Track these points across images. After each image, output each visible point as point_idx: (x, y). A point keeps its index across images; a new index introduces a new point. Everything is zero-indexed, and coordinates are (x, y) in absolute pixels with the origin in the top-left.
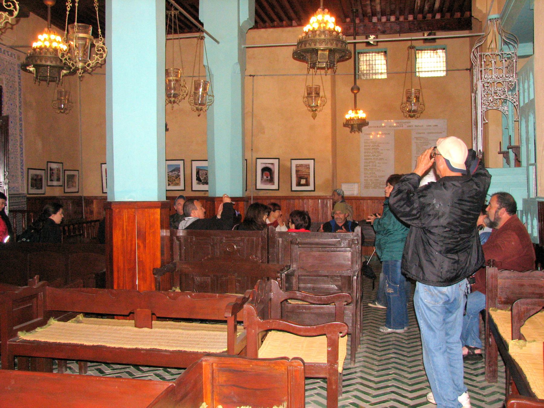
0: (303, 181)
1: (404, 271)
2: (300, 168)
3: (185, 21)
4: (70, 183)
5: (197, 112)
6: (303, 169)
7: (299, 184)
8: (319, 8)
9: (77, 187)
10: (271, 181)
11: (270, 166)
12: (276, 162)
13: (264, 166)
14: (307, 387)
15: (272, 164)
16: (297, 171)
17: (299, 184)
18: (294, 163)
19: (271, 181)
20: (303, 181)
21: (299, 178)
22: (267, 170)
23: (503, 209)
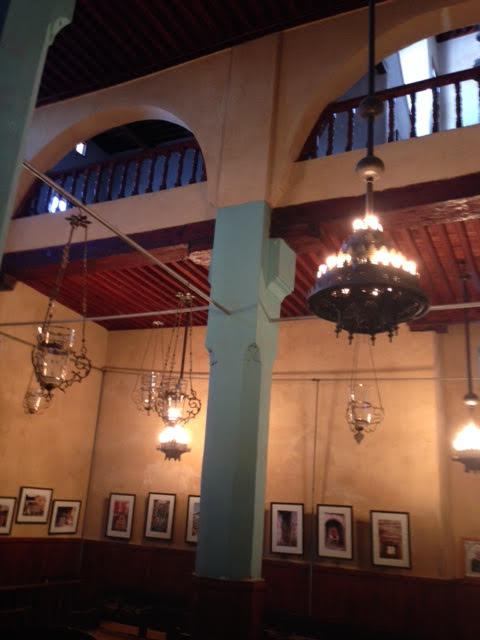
0: (391, 550)
1: (299, 288)
2: (385, 528)
3: (173, 282)
4: (62, 520)
5: (151, 411)
6: (391, 529)
7: (384, 554)
8: (369, 265)
9: (75, 525)
10: (341, 544)
11: (339, 518)
12: (347, 512)
13: (329, 517)
14: (405, 134)
15: (342, 515)
16: (381, 532)
17: (384, 554)
18: (377, 517)
19: (341, 544)
20: (391, 550)
21: (385, 544)
22: (334, 525)
23: (55, 304)
